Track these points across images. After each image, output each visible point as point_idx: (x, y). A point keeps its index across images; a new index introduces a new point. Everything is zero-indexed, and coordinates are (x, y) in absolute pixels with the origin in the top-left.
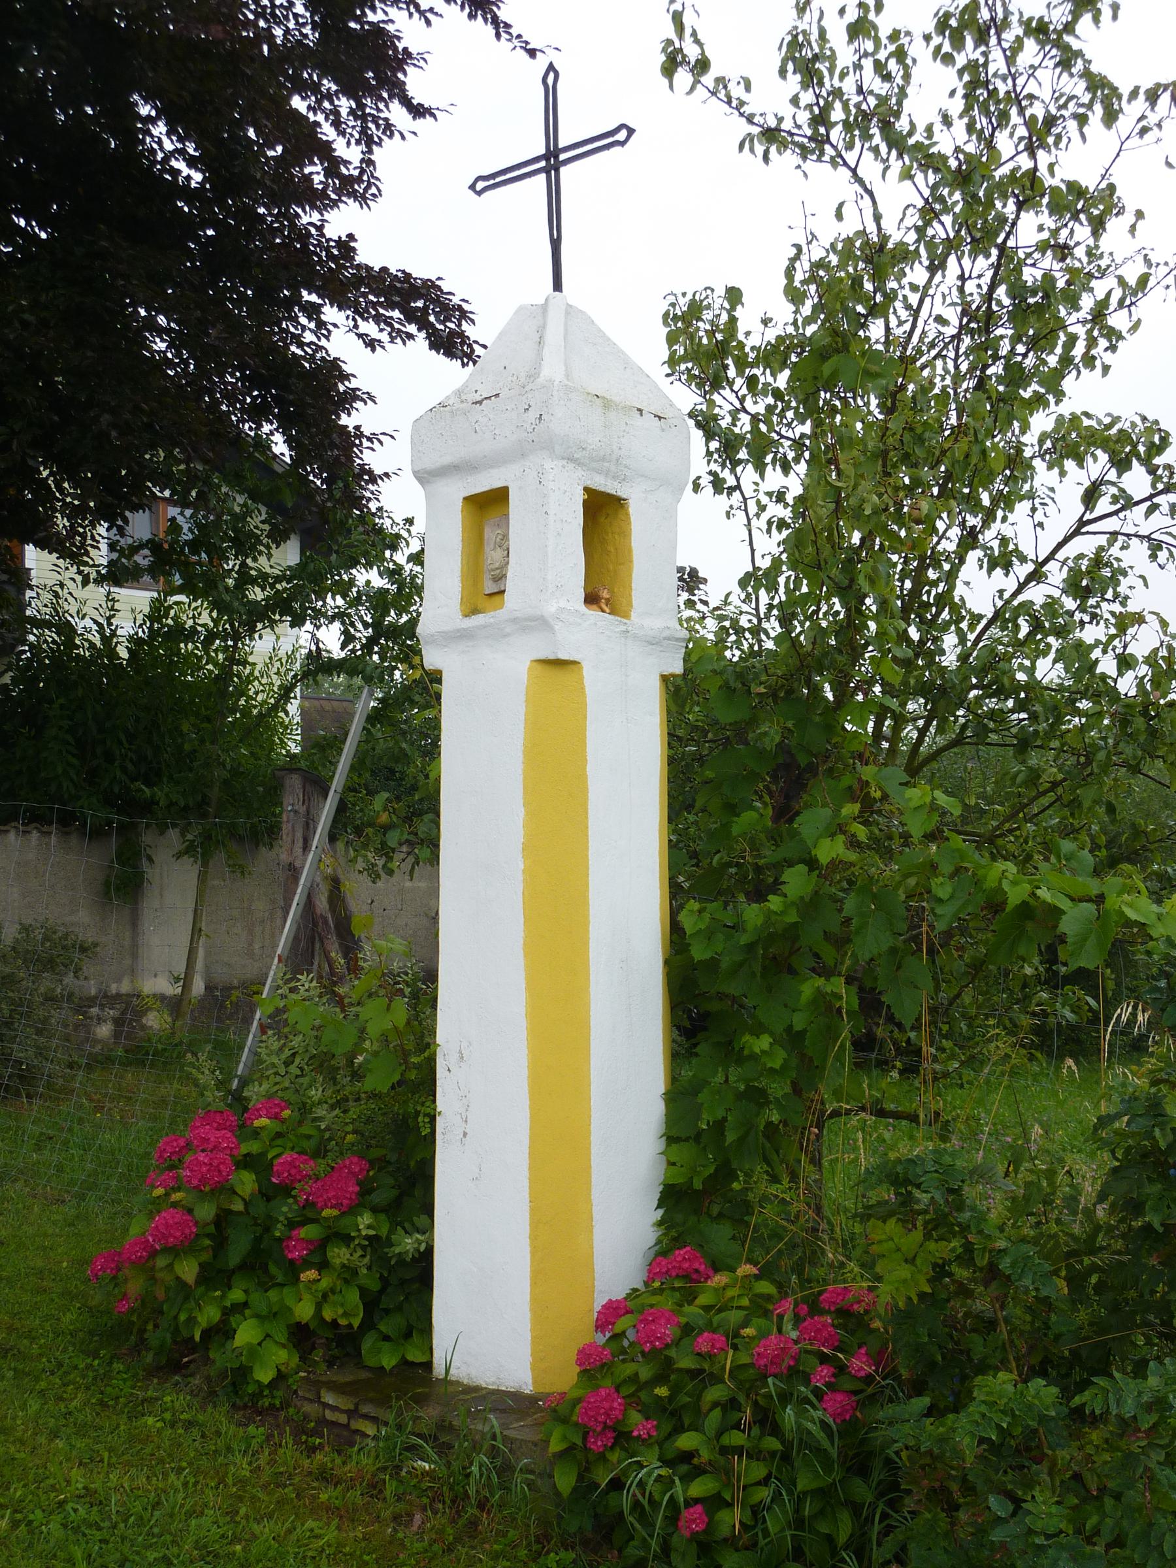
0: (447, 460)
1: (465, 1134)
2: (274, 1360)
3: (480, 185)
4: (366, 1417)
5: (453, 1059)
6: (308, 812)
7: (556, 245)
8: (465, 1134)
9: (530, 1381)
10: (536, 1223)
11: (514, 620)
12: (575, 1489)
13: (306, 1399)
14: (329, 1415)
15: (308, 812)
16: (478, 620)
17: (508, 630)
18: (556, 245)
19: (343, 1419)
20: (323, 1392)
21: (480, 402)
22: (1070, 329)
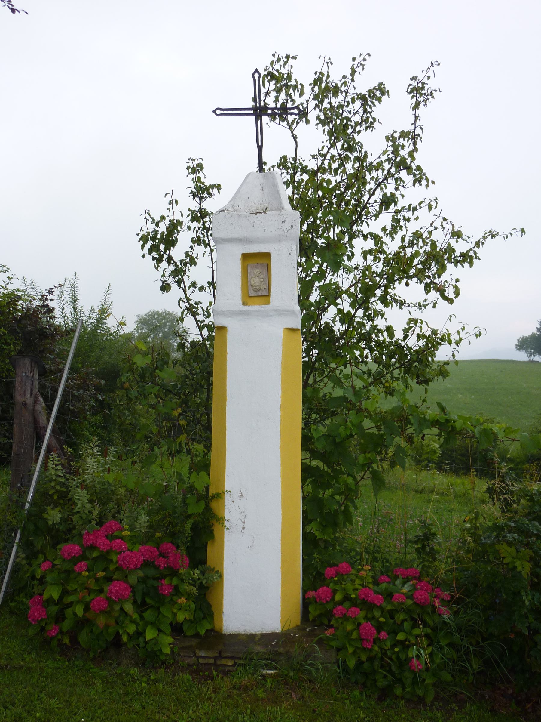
0: (236, 236)
1: (243, 528)
2: (167, 643)
3: (218, 112)
4: (226, 658)
5: (236, 496)
6: (33, 376)
7: (260, 149)
8: (243, 528)
9: (280, 627)
10: (283, 561)
11: (276, 310)
12: (356, 665)
13: (185, 656)
14: (201, 661)
15: (33, 376)
16: (246, 308)
17: (271, 314)
18: (260, 149)
19: (212, 661)
20: (197, 651)
21: (256, 214)
22: (195, 166)
